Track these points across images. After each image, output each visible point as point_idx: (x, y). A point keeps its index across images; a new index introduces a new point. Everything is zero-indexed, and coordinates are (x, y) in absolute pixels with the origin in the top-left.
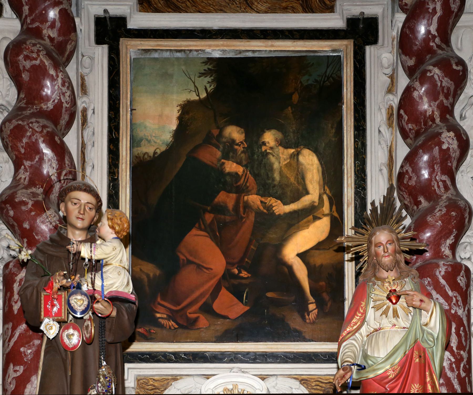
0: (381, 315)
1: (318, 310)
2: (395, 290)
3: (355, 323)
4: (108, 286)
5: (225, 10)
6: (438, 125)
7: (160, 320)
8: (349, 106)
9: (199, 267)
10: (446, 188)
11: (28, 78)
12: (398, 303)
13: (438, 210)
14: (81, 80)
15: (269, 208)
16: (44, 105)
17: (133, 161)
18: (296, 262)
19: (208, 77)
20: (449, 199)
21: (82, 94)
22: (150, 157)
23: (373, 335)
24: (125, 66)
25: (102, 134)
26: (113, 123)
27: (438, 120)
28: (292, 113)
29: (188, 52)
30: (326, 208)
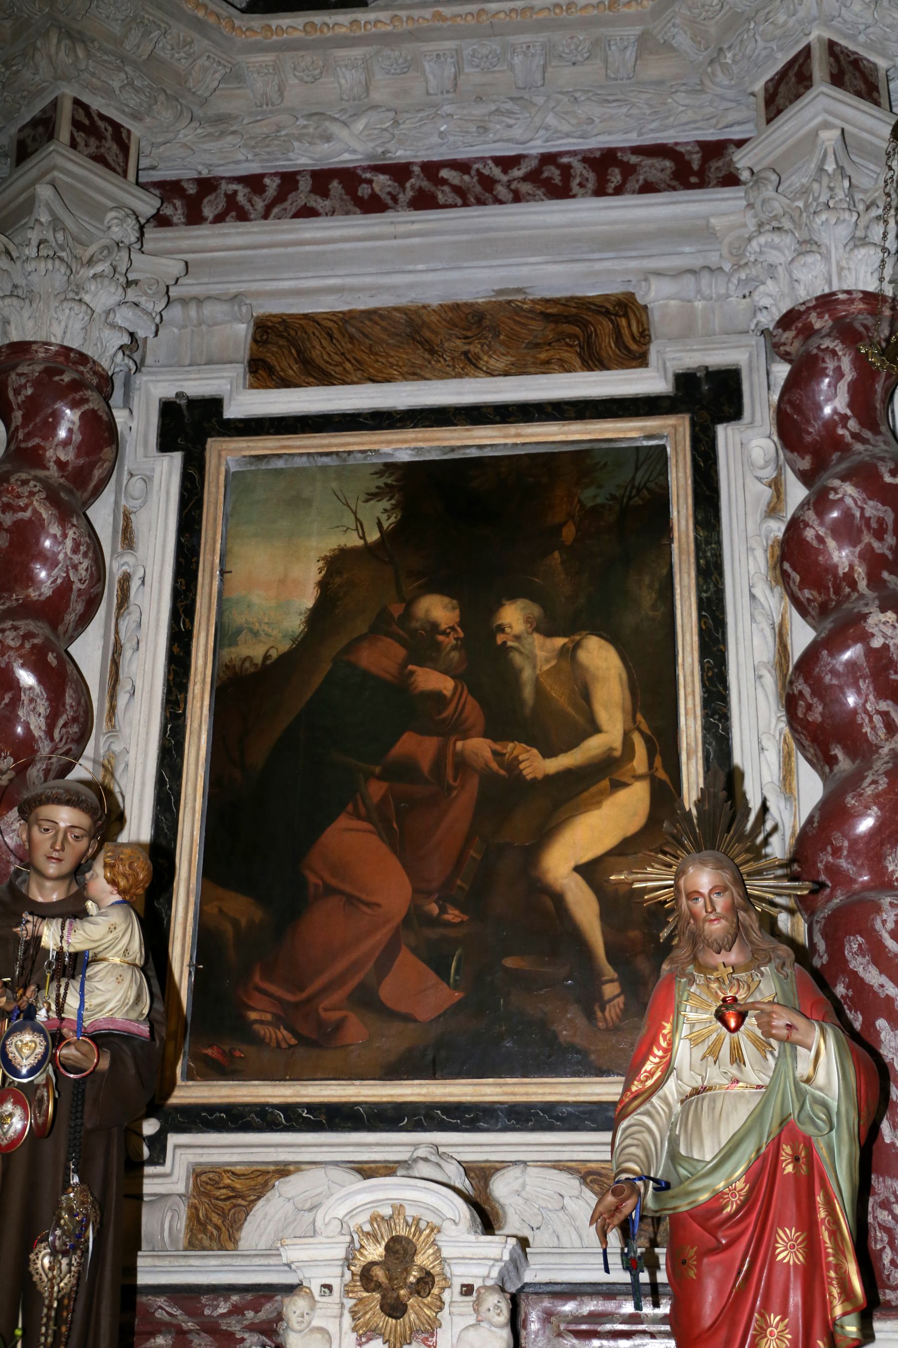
0: (704, 1057)
1: (626, 998)
2: (735, 999)
3: (649, 1072)
4: (92, 1008)
5: (422, 373)
6: (862, 596)
7: (257, 1027)
8: (684, 546)
9: (351, 900)
11: (7, 544)
12: (742, 1028)
13: (868, 780)
14: (124, 520)
15: (513, 766)
16: (34, 591)
17: (218, 675)
18: (572, 884)
19: (385, 500)
21: (122, 547)
22: (256, 665)
23: (691, 1102)
24: (213, 490)
25: (157, 626)
26: (181, 602)
27: (862, 585)
28: (563, 562)
29: (346, 455)
30: (640, 762)
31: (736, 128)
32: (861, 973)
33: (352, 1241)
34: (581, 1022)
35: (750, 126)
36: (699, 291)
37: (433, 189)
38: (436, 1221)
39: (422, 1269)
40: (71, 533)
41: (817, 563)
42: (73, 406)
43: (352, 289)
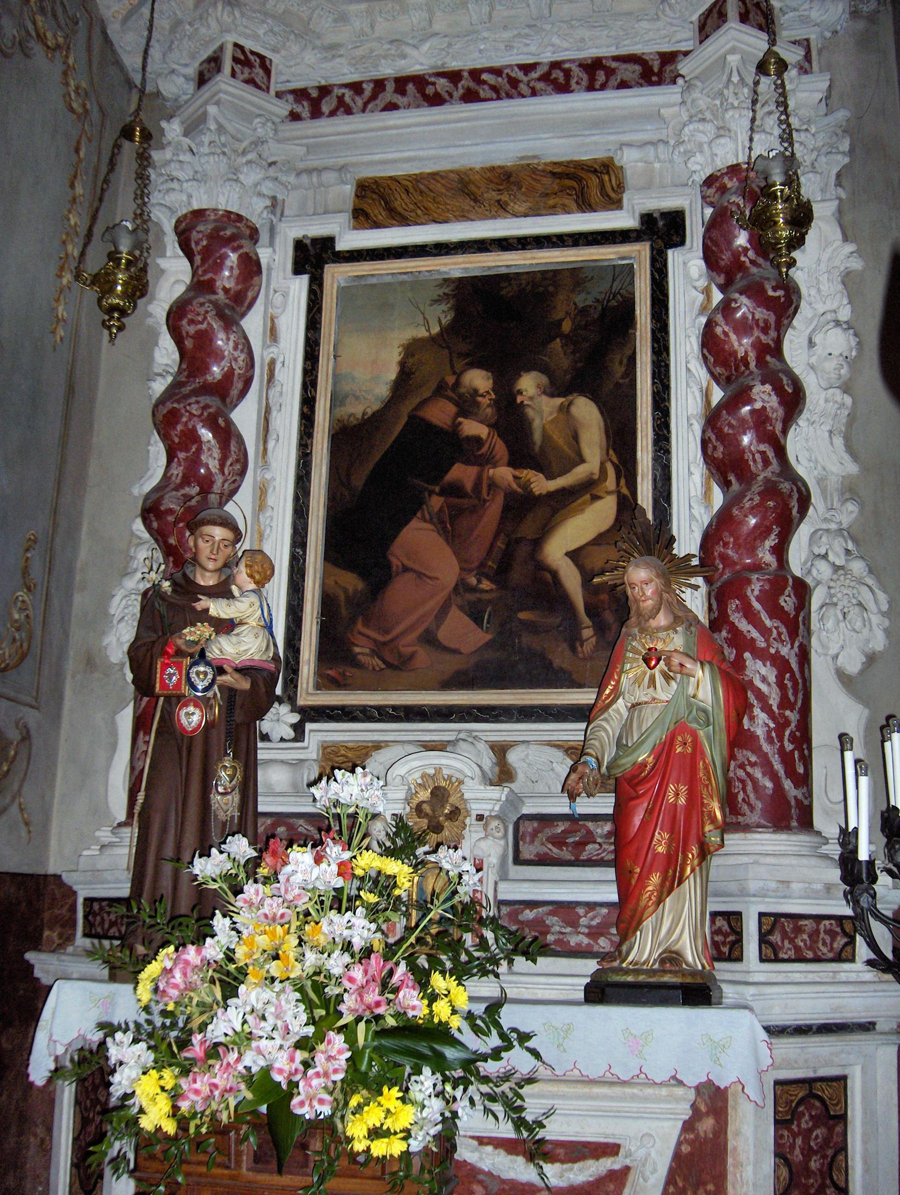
6: (751, 373)
7: (360, 657)
9: (420, 575)
10: (766, 462)
15: (526, 486)
20: (767, 480)
25: (293, 395)
27: (753, 365)
30: (611, 482)
31: (684, 44)
32: (737, 624)
33: (410, 789)
34: (568, 653)
35: (691, 43)
36: (657, 157)
37: (477, 87)
38: (461, 777)
39: (452, 805)
40: (232, 337)
41: (723, 350)
42: (234, 250)
43: (421, 159)
